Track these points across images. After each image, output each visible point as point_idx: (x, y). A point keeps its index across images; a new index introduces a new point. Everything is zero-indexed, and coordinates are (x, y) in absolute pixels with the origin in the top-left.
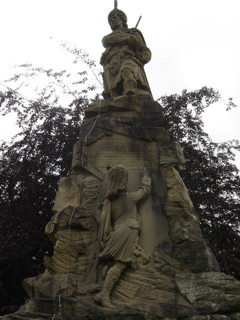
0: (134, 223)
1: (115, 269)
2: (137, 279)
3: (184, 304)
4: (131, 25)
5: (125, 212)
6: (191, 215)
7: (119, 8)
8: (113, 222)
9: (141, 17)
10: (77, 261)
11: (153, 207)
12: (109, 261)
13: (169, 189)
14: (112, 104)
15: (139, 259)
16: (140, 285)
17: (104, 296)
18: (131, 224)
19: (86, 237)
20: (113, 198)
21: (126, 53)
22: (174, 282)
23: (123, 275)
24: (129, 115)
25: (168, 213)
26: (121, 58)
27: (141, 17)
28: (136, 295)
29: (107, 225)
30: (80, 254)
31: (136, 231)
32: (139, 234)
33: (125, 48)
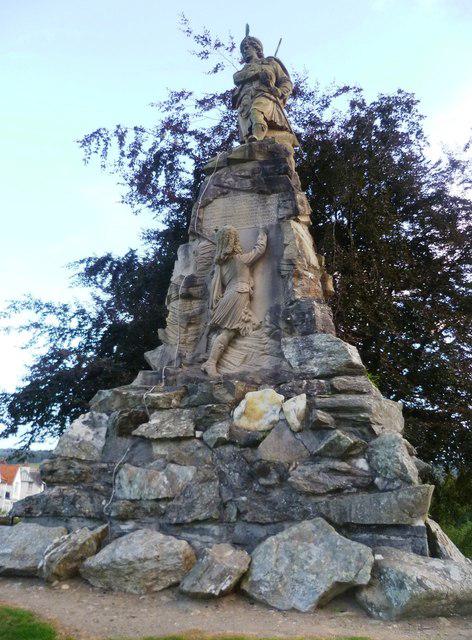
0: (245, 287)
1: (218, 340)
2: (245, 346)
3: (105, 551)
4: (267, 53)
5: (235, 275)
6: (305, 272)
7: (251, 34)
8: (224, 287)
9: (248, 27)
10: (186, 332)
11: (45, 360)
12: (216, 329)
13: (286, 245)
14: (231, 156)
15: (248, 325)
16: (248, 351)
17: (210, 366)
18: (239, 289)
19: (196, 305)
20: (222, 262)
21: (258, 90)
22: (280, 347)
23: (231, 342)
24: (249, 166)
25: (283, 273)
26: (252, 97)
27: (248, 27)
28: (244, 361)
29: (216, 292)
30: (189, 324)
31: (246, 296)
32: (251, 298)
33: (256, 85)
